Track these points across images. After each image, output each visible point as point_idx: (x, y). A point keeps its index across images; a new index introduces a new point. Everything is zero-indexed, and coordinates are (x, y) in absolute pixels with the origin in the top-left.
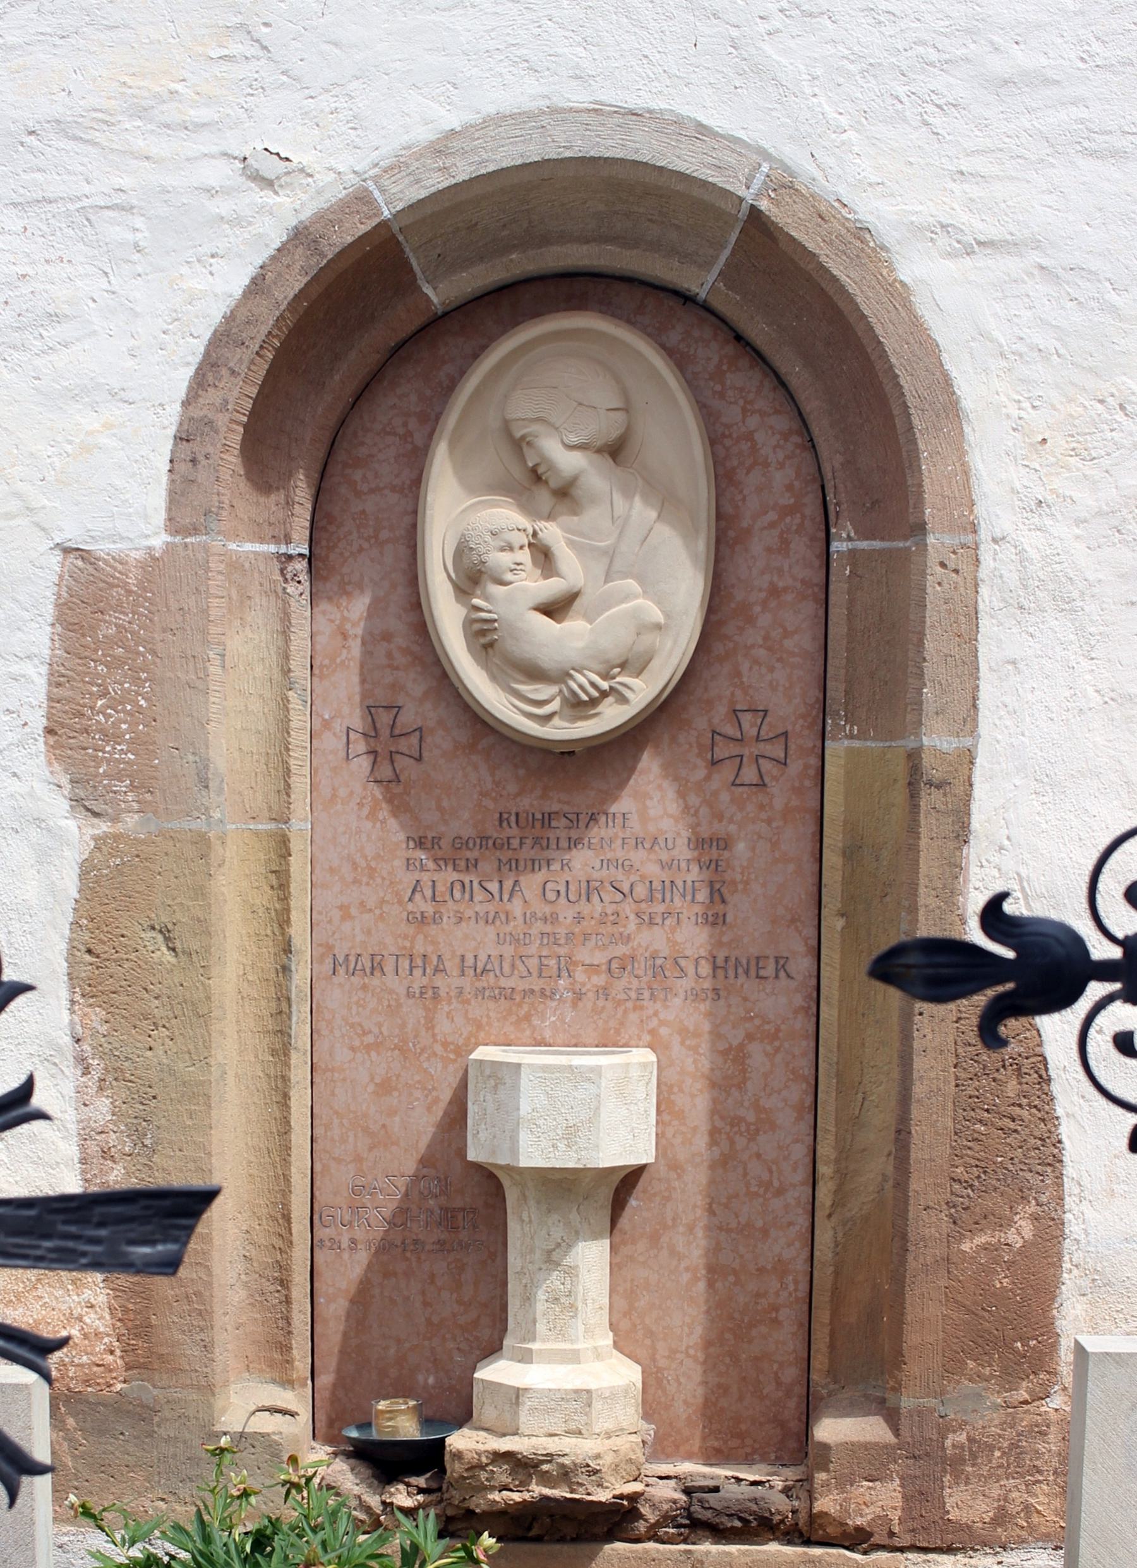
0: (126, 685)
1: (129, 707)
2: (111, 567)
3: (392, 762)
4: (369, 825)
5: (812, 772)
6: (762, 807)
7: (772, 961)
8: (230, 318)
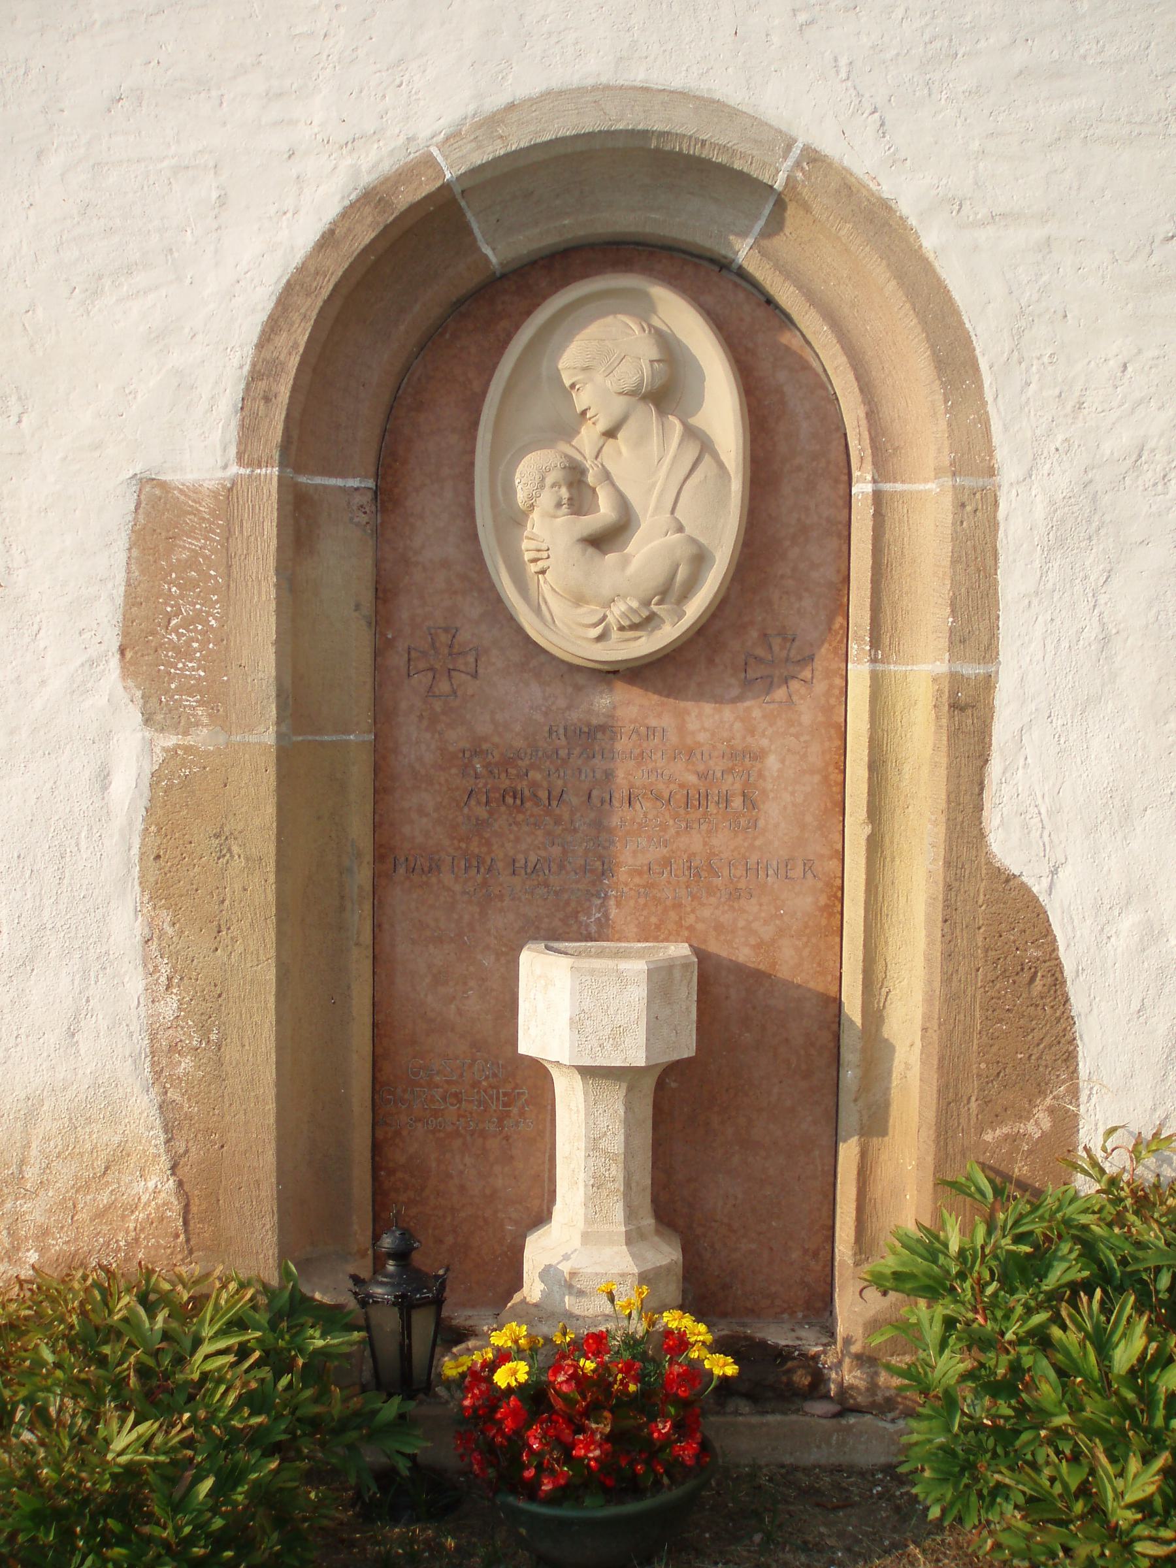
0: (198, 606)
1: (200, 627)
2: (186, 495)
3: (450, 678)
4: (428, 736)
5: (836, 692)
6: (791, 723)
7: (800, 863)
8: (302, 269)
